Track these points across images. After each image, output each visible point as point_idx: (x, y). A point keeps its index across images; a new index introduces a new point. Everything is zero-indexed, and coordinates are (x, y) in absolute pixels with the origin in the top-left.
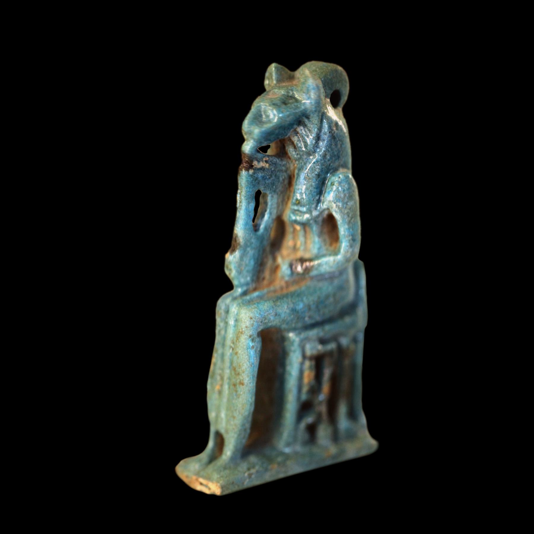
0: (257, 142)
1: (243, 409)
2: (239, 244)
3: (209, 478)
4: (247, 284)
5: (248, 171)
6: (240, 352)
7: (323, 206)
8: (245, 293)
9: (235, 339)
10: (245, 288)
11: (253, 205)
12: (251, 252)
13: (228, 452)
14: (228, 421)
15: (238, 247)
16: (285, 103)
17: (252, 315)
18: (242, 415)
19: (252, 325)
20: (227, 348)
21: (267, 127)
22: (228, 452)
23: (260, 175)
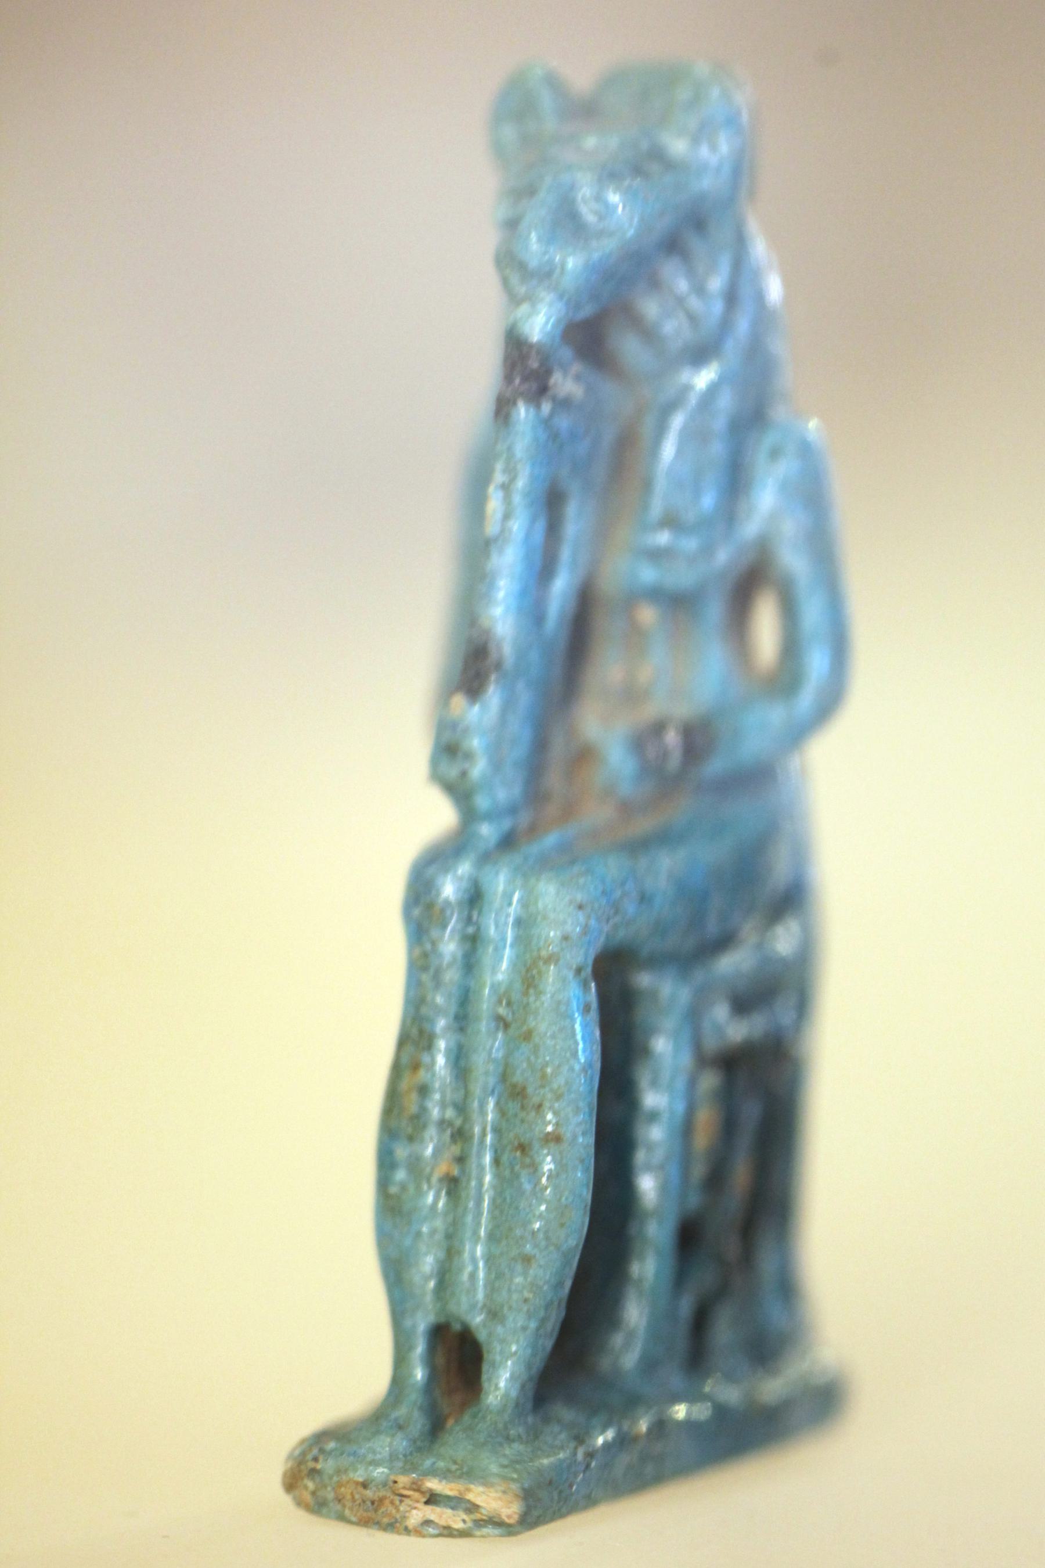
0: (568, 303)
1: (562, 1225)
2: (498, 666)
3: (468, 1473)
4: (513, 810)
5: (538, 406)
6: (543, 1027)
7: (750, 528)
8: (508, 842)
9: (518, 986)
10: (506, 824)
11: (541, 525)
12: (525, 697)
13: (503, 1379)
14: (497, 1276)
15: (493, 677)
16: (638, 170)
17: (579, 897)
18: (558, 1248)
19: (586, 930)
20: (484, 1026)
21: (606, 247)
22: (503, 1379)
23: (564, 423)
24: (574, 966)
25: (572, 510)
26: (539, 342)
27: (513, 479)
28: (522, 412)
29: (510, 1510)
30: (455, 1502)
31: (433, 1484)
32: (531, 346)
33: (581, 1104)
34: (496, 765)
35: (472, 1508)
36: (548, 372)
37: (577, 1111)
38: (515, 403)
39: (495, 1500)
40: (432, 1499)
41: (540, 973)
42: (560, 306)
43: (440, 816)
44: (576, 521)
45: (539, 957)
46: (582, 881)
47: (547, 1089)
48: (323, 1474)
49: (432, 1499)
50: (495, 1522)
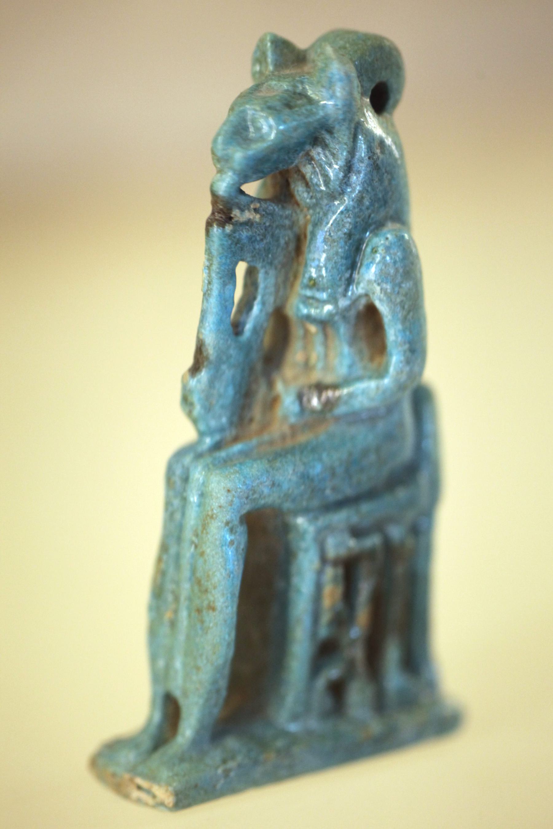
0: (239, 175)
1: (214, 653)
2: (207, 358)
3: (153, 778)
4: (222, 430)
5: (224, 227)
6: (208, 551)
7: (358, 290)
10: (217, 437)
13: (187, 730)
14: (187, 676)
17: (229, 485)
19: (231, 503)
23: (244, 234)
24: (225, 521)
25: (261, 276)
26: (225, 195)
27: (211, 264)
28: (216, 230)
29: (170, 800)
30: (148, 791)
31: (139, 781)
33: (225, 592)
35: (154, 797)
36: (230, 210)
37: (223, 595)
39: (163, 794)
40: (139, 788)
41: (208, 523)
43: (185, 433)
45: (208, 515)
46: (233, 476)
47: (209, 583)
48: (112, 763)
49: (139, 788)
50: (162, 804)
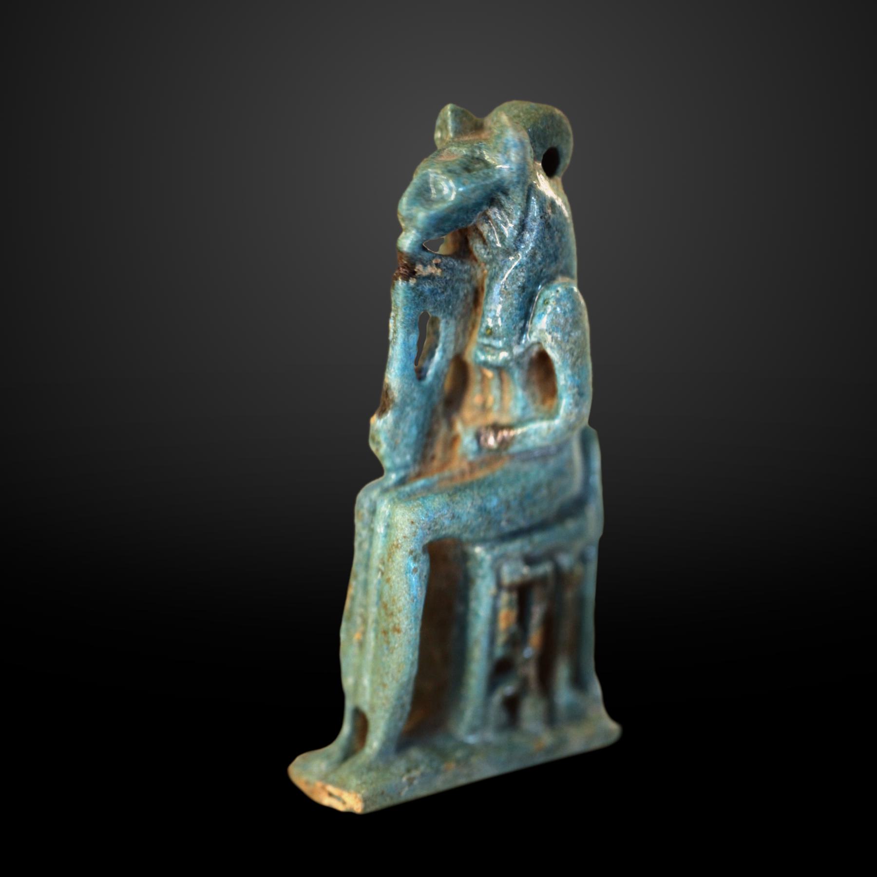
0: (422, 233)
1: (399, 671)
2: (393, 401)
3: (343, 786)
4: (406, 466)
5: (408, 281)
6: (394, 577)
7: (531, 338)
8: (402, 482)
9: (386, 556)
10: (402, 473)
12: (412, 414)
13: (375, 742)
14: (374, 692)
15: (391, 406)
16: (467, 169)
17: (413, 517)
18: (397, 682)
19: (415, 534)
20: (373, 572)
21: (438, 208)
22: (375, 742)
23: (427, 287)
32: (402, 253)
34: (394, 447)
38: (397, 279)
42: (419, 235)
44: (446, 330)
